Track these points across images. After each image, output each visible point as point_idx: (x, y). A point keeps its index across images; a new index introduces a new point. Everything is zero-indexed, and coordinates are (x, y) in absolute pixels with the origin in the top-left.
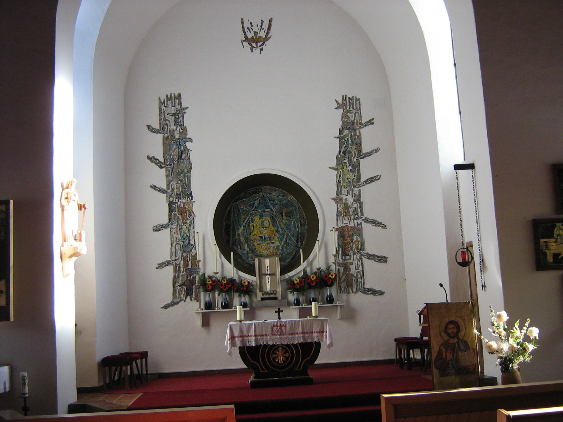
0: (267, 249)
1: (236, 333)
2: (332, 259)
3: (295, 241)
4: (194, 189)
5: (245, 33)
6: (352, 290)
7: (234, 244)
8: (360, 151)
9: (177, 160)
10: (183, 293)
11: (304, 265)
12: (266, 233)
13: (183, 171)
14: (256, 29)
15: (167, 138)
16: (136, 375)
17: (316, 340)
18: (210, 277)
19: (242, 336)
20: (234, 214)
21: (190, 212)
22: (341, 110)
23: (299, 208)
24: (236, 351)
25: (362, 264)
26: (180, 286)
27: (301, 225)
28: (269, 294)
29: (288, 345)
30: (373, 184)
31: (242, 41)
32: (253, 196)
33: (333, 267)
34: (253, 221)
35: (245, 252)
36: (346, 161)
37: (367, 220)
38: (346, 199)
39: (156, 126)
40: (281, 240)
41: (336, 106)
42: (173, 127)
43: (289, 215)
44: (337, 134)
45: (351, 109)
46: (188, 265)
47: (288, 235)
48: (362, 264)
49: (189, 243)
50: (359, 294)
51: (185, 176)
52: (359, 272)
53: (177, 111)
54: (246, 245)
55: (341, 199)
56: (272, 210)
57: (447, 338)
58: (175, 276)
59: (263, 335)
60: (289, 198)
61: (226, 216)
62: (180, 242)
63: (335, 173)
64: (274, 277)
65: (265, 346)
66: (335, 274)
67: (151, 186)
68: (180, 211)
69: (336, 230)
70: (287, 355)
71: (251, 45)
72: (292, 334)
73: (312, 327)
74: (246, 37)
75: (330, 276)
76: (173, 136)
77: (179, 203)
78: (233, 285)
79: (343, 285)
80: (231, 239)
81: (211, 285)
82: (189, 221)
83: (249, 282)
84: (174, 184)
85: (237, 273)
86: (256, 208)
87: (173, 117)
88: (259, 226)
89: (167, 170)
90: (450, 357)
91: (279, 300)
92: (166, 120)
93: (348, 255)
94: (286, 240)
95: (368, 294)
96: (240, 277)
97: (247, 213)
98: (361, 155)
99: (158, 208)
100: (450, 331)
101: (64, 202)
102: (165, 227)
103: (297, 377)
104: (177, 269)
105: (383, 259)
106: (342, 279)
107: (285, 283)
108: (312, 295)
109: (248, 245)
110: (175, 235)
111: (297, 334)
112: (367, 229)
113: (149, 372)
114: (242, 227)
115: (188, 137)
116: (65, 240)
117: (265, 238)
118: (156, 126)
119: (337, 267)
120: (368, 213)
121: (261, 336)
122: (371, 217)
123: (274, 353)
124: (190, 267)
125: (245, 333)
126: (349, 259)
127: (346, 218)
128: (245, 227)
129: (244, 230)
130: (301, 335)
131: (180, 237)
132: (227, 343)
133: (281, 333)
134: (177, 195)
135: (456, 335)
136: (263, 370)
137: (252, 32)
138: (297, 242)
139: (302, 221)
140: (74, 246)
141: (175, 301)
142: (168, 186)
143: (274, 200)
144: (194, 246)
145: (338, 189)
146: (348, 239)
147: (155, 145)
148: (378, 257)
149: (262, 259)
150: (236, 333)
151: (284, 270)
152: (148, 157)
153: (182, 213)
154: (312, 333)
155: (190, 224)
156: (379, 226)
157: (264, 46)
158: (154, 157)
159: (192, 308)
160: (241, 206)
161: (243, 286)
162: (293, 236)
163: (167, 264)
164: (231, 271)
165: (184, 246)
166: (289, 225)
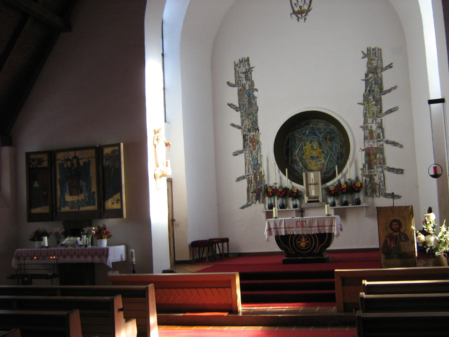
0: (316, 165)
1: (272, 226)
2: (360, 172)
3: (336, 159)
4: (260, 125)
5: (293, 8)
6: (376, 195)
7: (292, 162)
8: (381, 89)
9: (248, 105)
10: (254, 198)
11: (338, 177)
12: (315, 154)
13: (252, 113)
14: (301, 4)
15: (241, 90)
16: (218, 254)
17: (327, 232)
18: (271, 187)
19: (276, 228)
20: (292, 140)
21: (257, 141)
22: (366, 59)
23: (339, 134)
24: (273, 238)
25: (384, 175)
26: (252, 193)
27: (341, 147)
28: (313, 198)
29: (307, 235)
30: (392, 114)
31: (291, 14)
32: (305, 127)
33: (360, 177)
34: (305, 145)
35: (300, 168)
36: (371, 97)
37: (387, 142)
38: (371, 127)
39: (233, 82)
40: (326, 159)
41: (362, 56)
42: (244, 82)
43: (332, 139)
44: (364, 77)
45: (374, 57)
46: (257, 178)
47: (331, 155)
48: (384, 175)
49: (257, 163)
50: (382, 197)
51: (253, 117)
52: (381, 181)
53: (246, 70)
54: (301, 163)
55: (367, 127)
56: (319, 137)
57: (391, 232)
58: (248, 186)
59: (290, 228)
60: (331, 128)
61: (286, 142)
62: (251, 163)
63: (362, 107)
64: (317, 186)
65: (293, 235)
66: (361, 184)
67: (231, 125)
68: (251, 141)
69: (363, 150)
70: (308, 242)
71: (297, 16)
72: (310, 227)
73: (324, 222)
74: (294, 11)
75: (357, 185)
76: (244, 88)
77: (250, 135)
78: (286, 192)
79: (369, 191)
80: (290, 158)
81: (271, 192)
82: (257, 148)
83: (297, 190)
84: (246, 122)
85: (291, 183)
86: (308, 136)
87: (244, 75)
88: (309, 149)
89: (241, 113)
90: (393, 245)
91: (321, 203)
92: (239, 77)
93: (373, 169)
94: (330, 158)
95: (388, 198)
96: (293, 186)
97: (301, 140)
98: (382, 92)
99: (236, 139)
100: (394, 227)
101: (156, 142)
102: (241, 152)
103: (315, 257)
104: (249, 182)
105: (400, 171)
106: (368, 187)
107: (324, 191)
108: (344, 199)
109: (302, 163)
110: (248, 158)
111: (314, 227)
112: (388, 148)
113: (230, 252)
114: (298, 150)
115: (255, 87)
116: (158, 167)
117: (314, 158)
118: (233, 82)
119: (364, 178)
120: (389, 136)
121: (289, 228)
122: (391, 139)
123: (299, 240)
124: (258, 180)
125: (278, 226)
126: (374, 172)
127: (371, 141)
128: (299, 150)
129: (299, 152)
130: (317, 228)
131: (251, 159)
132: (266, 233)
133: (303, 226)
134: (249, 129)
135: (398, 230)
136: (291, 251)
137: (298, 6)
138: (338, 159)
139: (341, 143)
140: (162, 170)
141: (249, 203)
142: (242, 123)
143: (320, 129)
144: (260, 165)
145: (365, 119)
146: (373, 157)
147: (233, 95)
148: (397, 169)
149: (309, 173)
150: (272, 226)
151: (324, 181)
152: (228, 104)
153: (252, 141)
154: (325, 226)
155: (258, 150)
156: (397, 146)
157: (307, 16)
158: (232, 104)
159: (259, 208)
160: (297, 135)
161: (293, 193)
162: (334, 155)
163: (243, 178)
164: (287, 183)
165: (254, 165)
166: (331, 147)
